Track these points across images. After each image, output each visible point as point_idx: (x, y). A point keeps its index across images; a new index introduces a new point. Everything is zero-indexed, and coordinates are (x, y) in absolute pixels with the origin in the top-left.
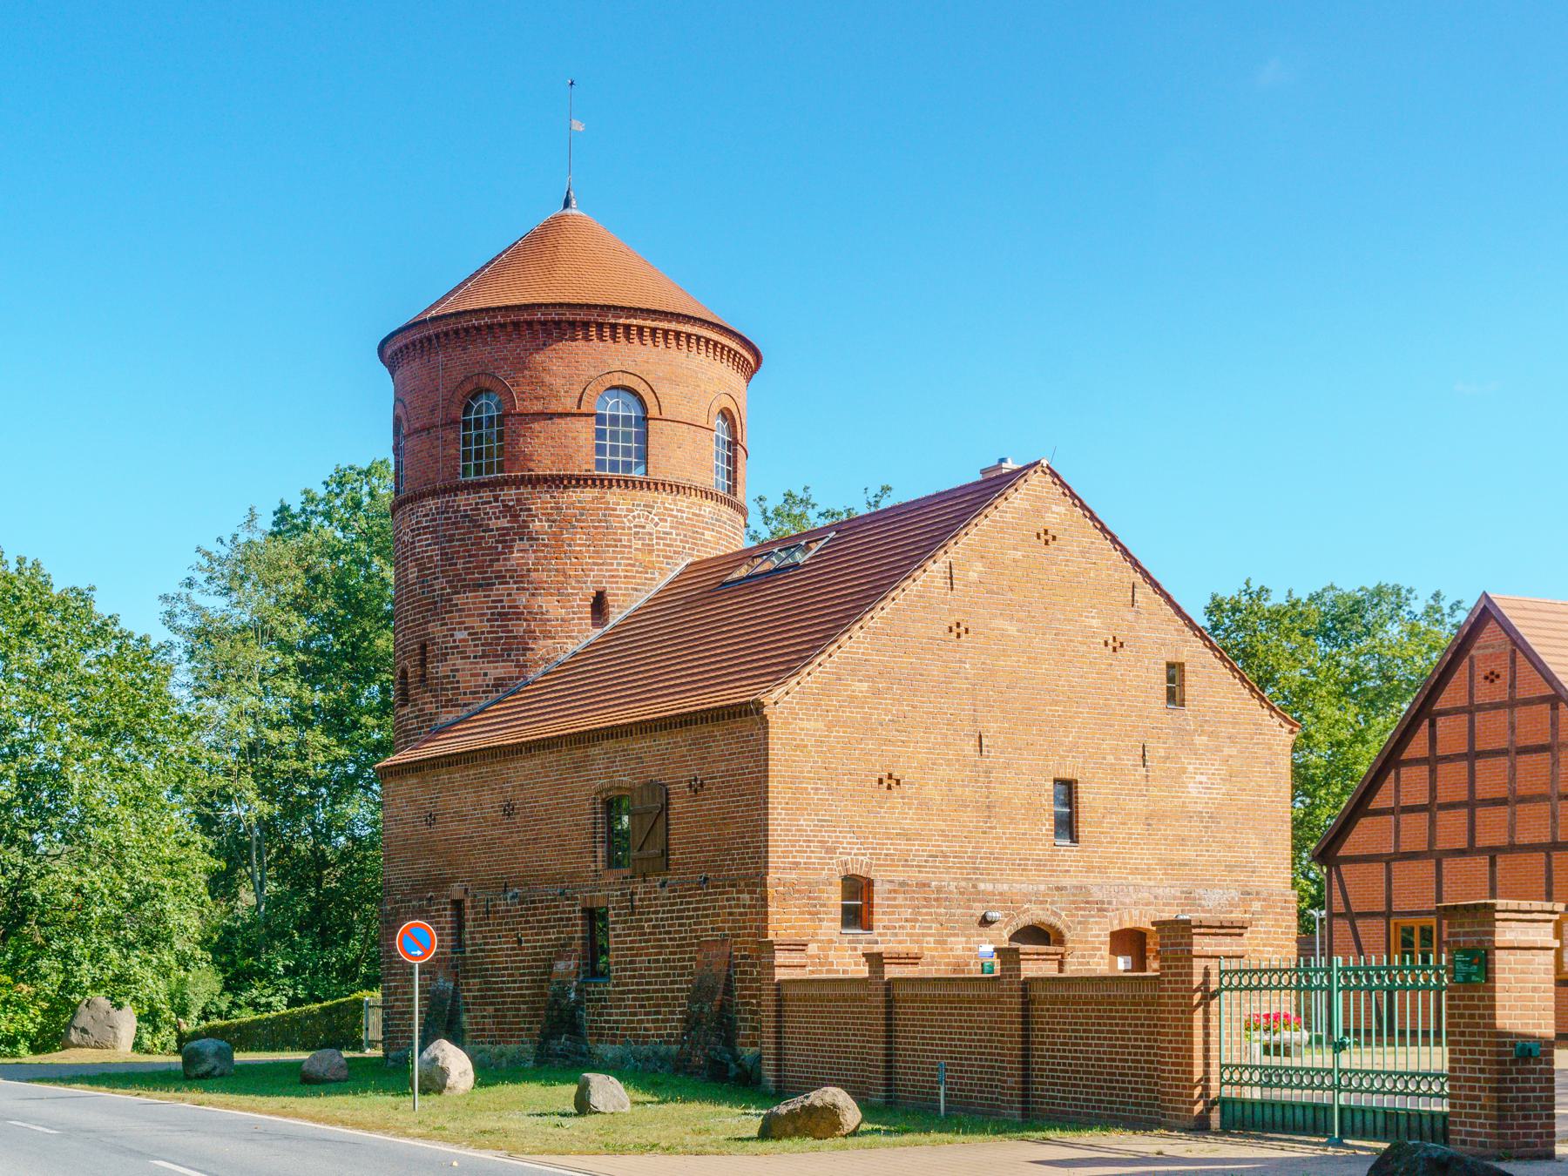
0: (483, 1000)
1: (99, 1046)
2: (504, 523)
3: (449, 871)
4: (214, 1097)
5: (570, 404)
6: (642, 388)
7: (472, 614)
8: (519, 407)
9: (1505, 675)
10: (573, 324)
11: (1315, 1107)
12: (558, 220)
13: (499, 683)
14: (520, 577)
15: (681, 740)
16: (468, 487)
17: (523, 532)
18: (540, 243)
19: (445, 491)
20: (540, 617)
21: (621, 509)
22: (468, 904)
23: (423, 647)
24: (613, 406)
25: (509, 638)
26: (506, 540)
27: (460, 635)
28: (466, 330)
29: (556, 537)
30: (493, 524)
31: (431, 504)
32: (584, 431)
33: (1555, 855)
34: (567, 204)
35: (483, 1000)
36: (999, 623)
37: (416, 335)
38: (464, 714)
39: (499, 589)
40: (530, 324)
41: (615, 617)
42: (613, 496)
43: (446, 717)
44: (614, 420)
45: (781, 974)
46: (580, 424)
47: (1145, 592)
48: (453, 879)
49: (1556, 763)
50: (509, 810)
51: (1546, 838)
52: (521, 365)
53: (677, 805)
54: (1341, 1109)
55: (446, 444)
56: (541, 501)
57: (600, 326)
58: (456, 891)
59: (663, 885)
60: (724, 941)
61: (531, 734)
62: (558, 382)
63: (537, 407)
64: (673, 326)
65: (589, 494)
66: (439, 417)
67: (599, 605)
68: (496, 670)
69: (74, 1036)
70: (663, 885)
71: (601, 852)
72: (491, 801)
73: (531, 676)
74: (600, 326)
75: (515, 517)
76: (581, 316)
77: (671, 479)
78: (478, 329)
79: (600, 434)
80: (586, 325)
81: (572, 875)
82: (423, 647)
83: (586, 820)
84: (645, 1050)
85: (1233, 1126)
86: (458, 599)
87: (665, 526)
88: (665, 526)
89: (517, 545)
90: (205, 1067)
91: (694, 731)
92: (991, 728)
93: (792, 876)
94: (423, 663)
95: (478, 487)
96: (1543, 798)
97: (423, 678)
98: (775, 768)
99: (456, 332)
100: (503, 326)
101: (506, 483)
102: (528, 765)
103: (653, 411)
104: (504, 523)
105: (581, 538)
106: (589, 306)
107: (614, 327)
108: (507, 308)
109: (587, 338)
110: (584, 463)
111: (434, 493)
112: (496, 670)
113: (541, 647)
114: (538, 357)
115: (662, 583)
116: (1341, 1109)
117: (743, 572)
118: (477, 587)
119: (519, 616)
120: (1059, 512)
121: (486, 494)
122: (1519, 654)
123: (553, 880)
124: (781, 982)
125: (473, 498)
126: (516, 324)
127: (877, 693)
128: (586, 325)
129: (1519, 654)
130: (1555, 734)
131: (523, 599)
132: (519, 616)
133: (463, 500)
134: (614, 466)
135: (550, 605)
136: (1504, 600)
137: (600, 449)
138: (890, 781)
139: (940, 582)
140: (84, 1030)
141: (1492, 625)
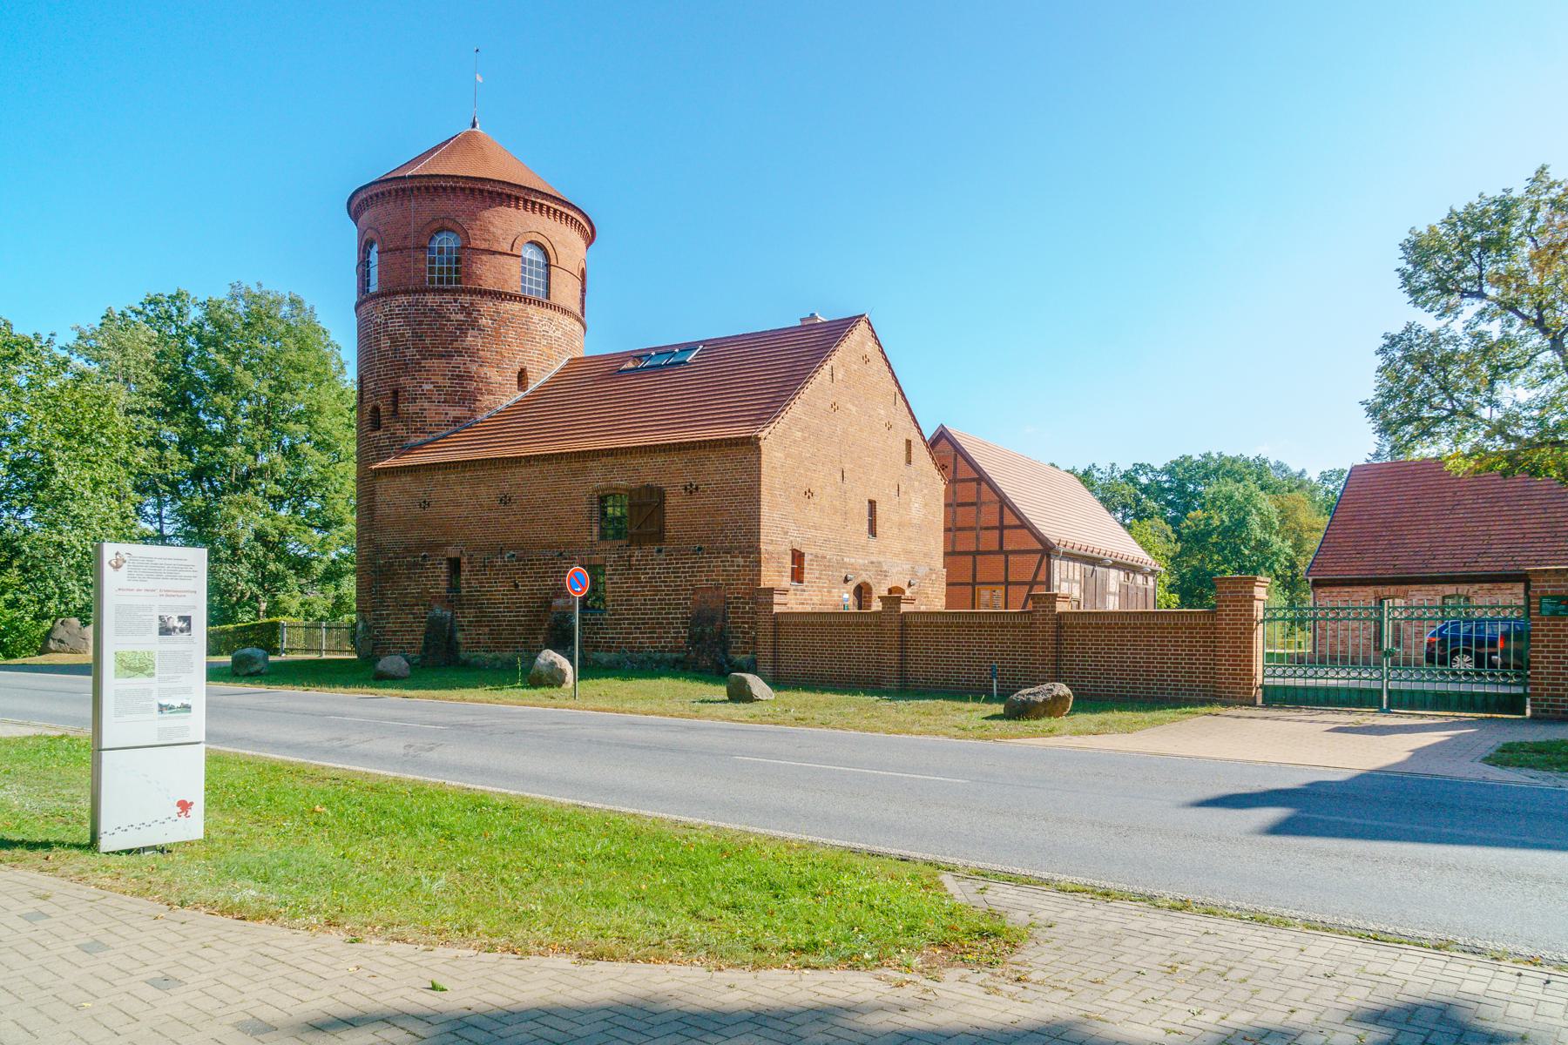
0: (478, 623)
1: (73, 651)
2: (461, 317)
3: (444, 540)
4: (390, 691)
5: (506, 247)
6: (548, 246)
7: (435, 376)
8: (473, 244)
9: (951, 467)
10: (509, 196)
11: (1371, 691)
12: (467, 135)
13: (456, 420)
14: (472, 353)
15: (678, 461)
16: (434, 291)
17: (474, 324)
18: (464, 142)
19: (415, 292)
20: (485, 380)
21: (536, 319)
22: (464, 560)
23: (395, 393)
24: (530, 253)
25: (464, 392)
26: (463, 328)
27: (426, 387)
28: (435, 188)
29: (497, 330)
30: (453, 317)
31: (403, 299)
32: (514, 266)
33: (978, 557)
34: (474, 125)
35: (478, 623)
36: (849, 406)
37: (387, 187)
38: (430, 438)
39: (457, 360)
40: (481, 191)
41: (532, 387)
42: (531, 310)
43: (415, 439)
44: (531, 262)
45: (776, 609)
46: (512, 260)
47: (899, 397)
48: (448, 544)
49: (979, 512)
50: (505, 500)
51: (973, 548)
52: (473, 216)
53: (672, 501)
54: (1390, 692)
55: (416, 261)
56: (486, 306)
57: (526, 201)
58: (452, 552)
59: (660, 551)
60: (717, 588)
61: (623, 442)
62: (498, 232)
63: (484, 246)
64: (565, 210)
65: (517, 306)
66: (411, 242)
67: (522, 377)
68: (454, 412)
69: (52, 645)
70: (660, 551)
71: (596, 530)
72: (486, 495)
73: (479, 418)
74: (526, 201)
75: (469, 314)
76: (515, 192)
77: (562, 305)
78: (445, 189)
79: (524, 269)
80: (517, 199)
81: (570, 544)
82: (395, 393)
83: (584, 508)
84: (641, 656)
85: (1274, 701)
86: (426, 363)
87: (559, 334)
88: (559, 334)
89: (470, 332)
90: (256, 668)
91: (691, 454)
92: (847, 467)
93: (770, 548)
94: (395, 403)
95: (443, 291)
96: (972, 529)
97: (395, 413)
98: (765, 480)
99: (427, 188)
100: (463, 189)
101: (464, 291)
102: (522, 472)
103: (553, 262)
104: (461, 317)
105: (512, 334)
106: (521, 187)
107: (534, 203)
108: (467, 178)
109: (517, 207)
110: (514, 286)
111: (406, 292)
112: (454, 412)
113: (486, 400)
114: (486, 214)
115: (557, 368)
116: (1390, 692)
117: (630, 365)
118: (441, 356)
119: (471, 378)
120: (870, 345)
121: (448, 297)
122: (959, 458)
123: (550, 547)
124: (905, 614)
125: (438, 299)
126: (472, 190)
127: (804, 439)
128: (517, 199)
129: (959, 458)
130: (979, 497)
131: (474, 368)
132: (471, 378)
133: (430, 299)
134: (530, 291)
135: (492, 374)
136: (954, 430)
137: (523, 280)
138: (809, 494)
139: (828, 377)
140: (61, 641)
141: (944, 441)
